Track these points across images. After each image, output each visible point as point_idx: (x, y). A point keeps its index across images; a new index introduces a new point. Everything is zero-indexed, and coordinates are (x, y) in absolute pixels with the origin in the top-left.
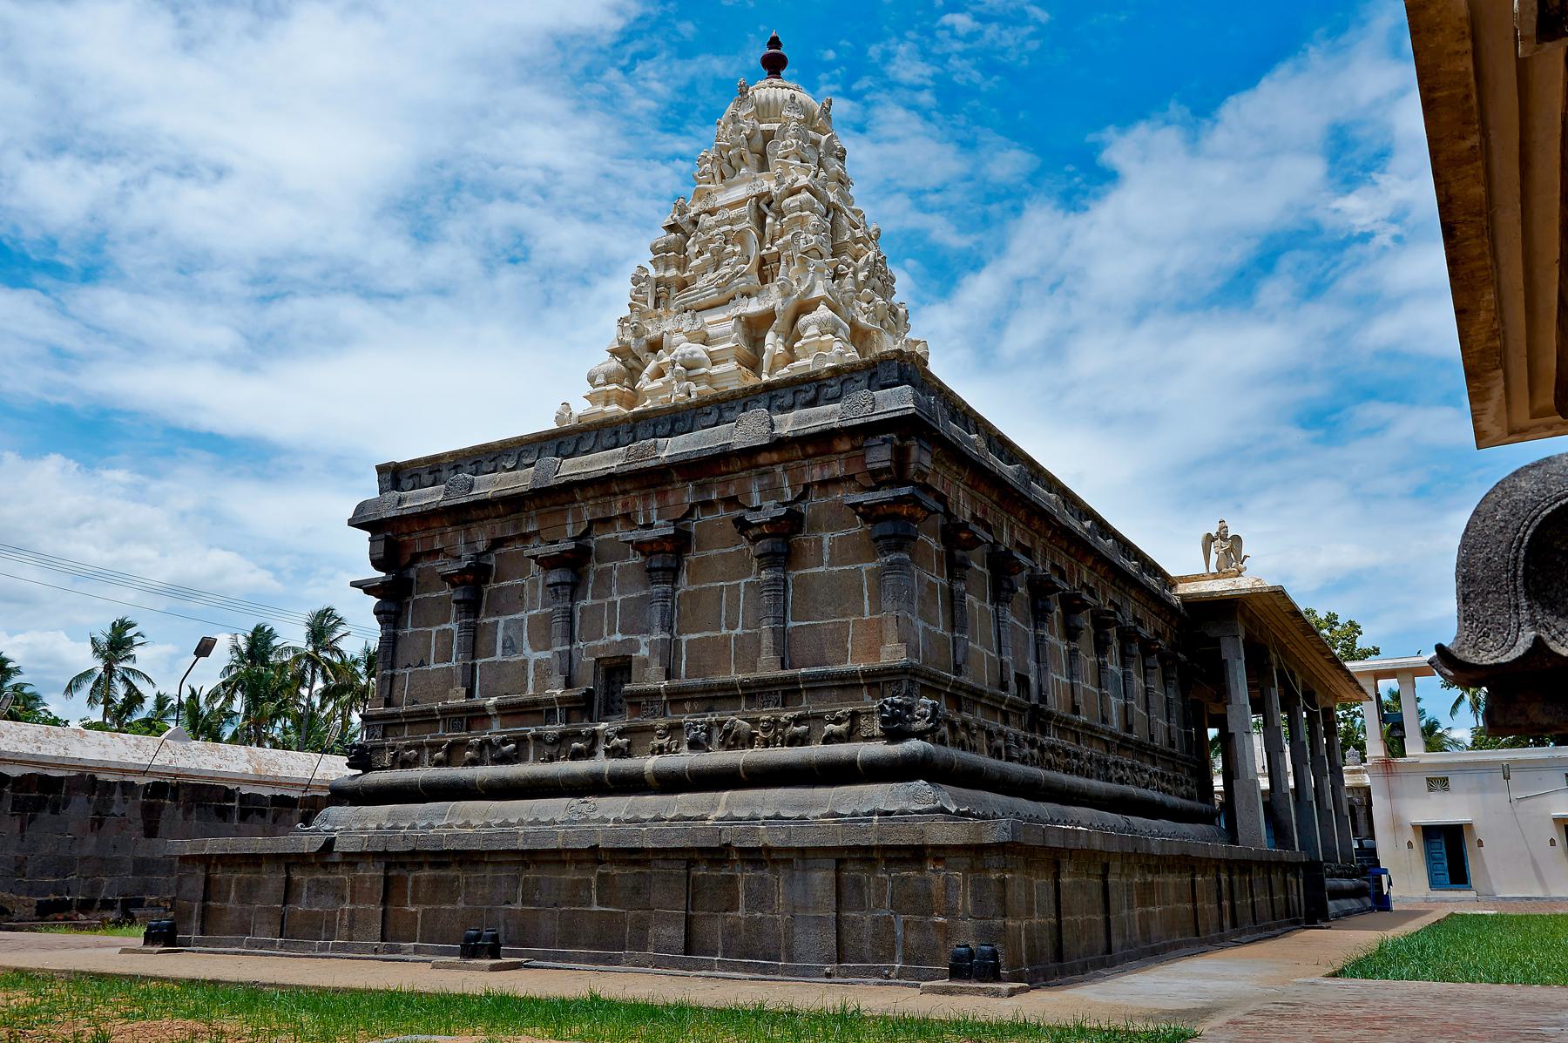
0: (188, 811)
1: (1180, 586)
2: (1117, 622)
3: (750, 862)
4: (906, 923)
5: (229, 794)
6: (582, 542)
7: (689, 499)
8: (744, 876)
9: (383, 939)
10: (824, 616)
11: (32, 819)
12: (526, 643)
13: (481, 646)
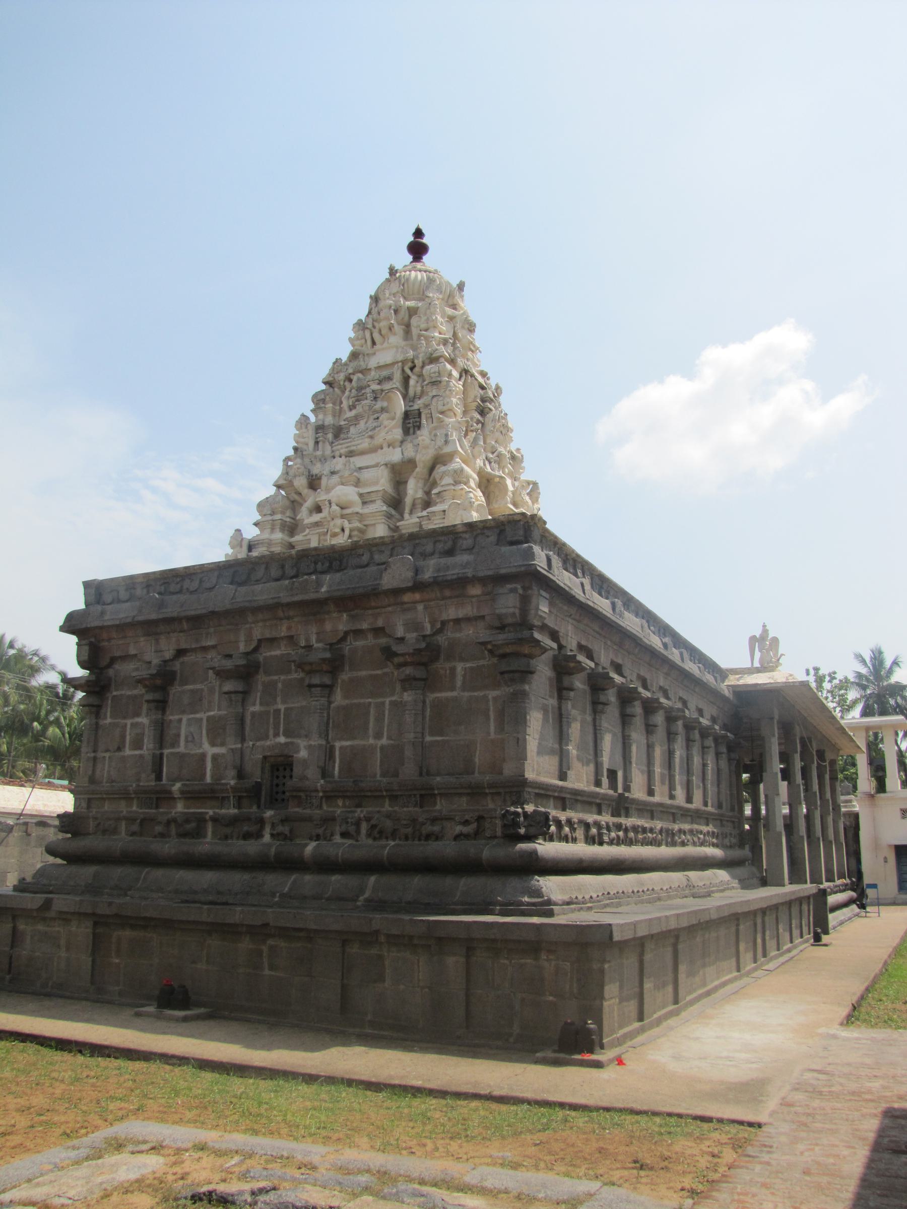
1: (731, 677)
2: (685, 717)
7: (342, 627)
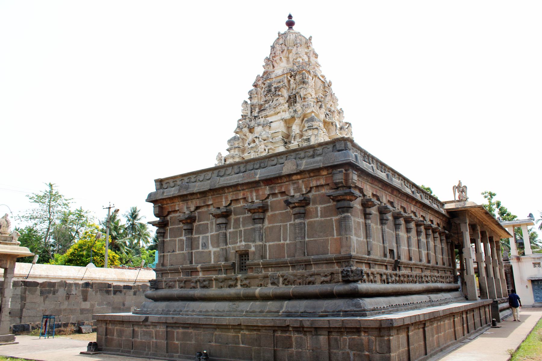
0: (96, 292)
3: (297, 331)
4: (354, 354)
5: (109, 286)
6: (228, 208)
7: (267, 192)
8: (295, 336)
9: (167, 352)
10: (319, 236)
11: (47, 297)
12: (210, 245)
13: (194, 246)
